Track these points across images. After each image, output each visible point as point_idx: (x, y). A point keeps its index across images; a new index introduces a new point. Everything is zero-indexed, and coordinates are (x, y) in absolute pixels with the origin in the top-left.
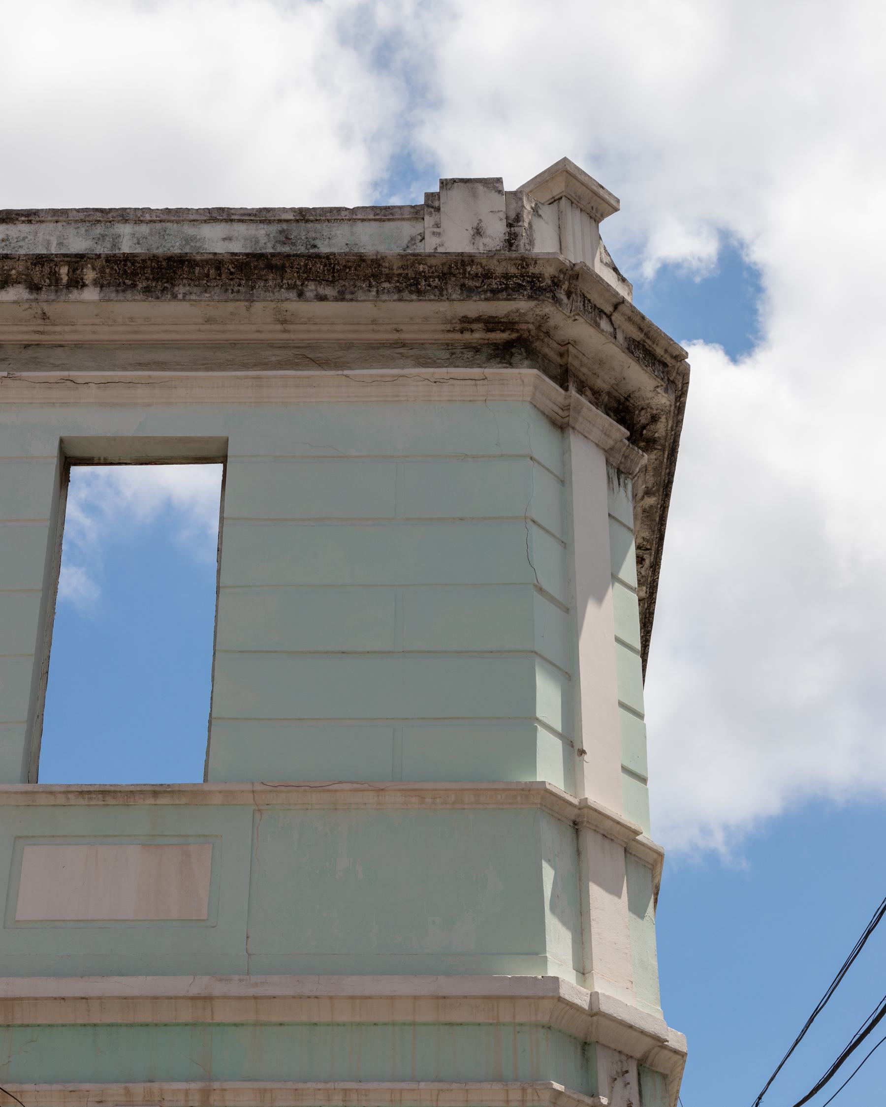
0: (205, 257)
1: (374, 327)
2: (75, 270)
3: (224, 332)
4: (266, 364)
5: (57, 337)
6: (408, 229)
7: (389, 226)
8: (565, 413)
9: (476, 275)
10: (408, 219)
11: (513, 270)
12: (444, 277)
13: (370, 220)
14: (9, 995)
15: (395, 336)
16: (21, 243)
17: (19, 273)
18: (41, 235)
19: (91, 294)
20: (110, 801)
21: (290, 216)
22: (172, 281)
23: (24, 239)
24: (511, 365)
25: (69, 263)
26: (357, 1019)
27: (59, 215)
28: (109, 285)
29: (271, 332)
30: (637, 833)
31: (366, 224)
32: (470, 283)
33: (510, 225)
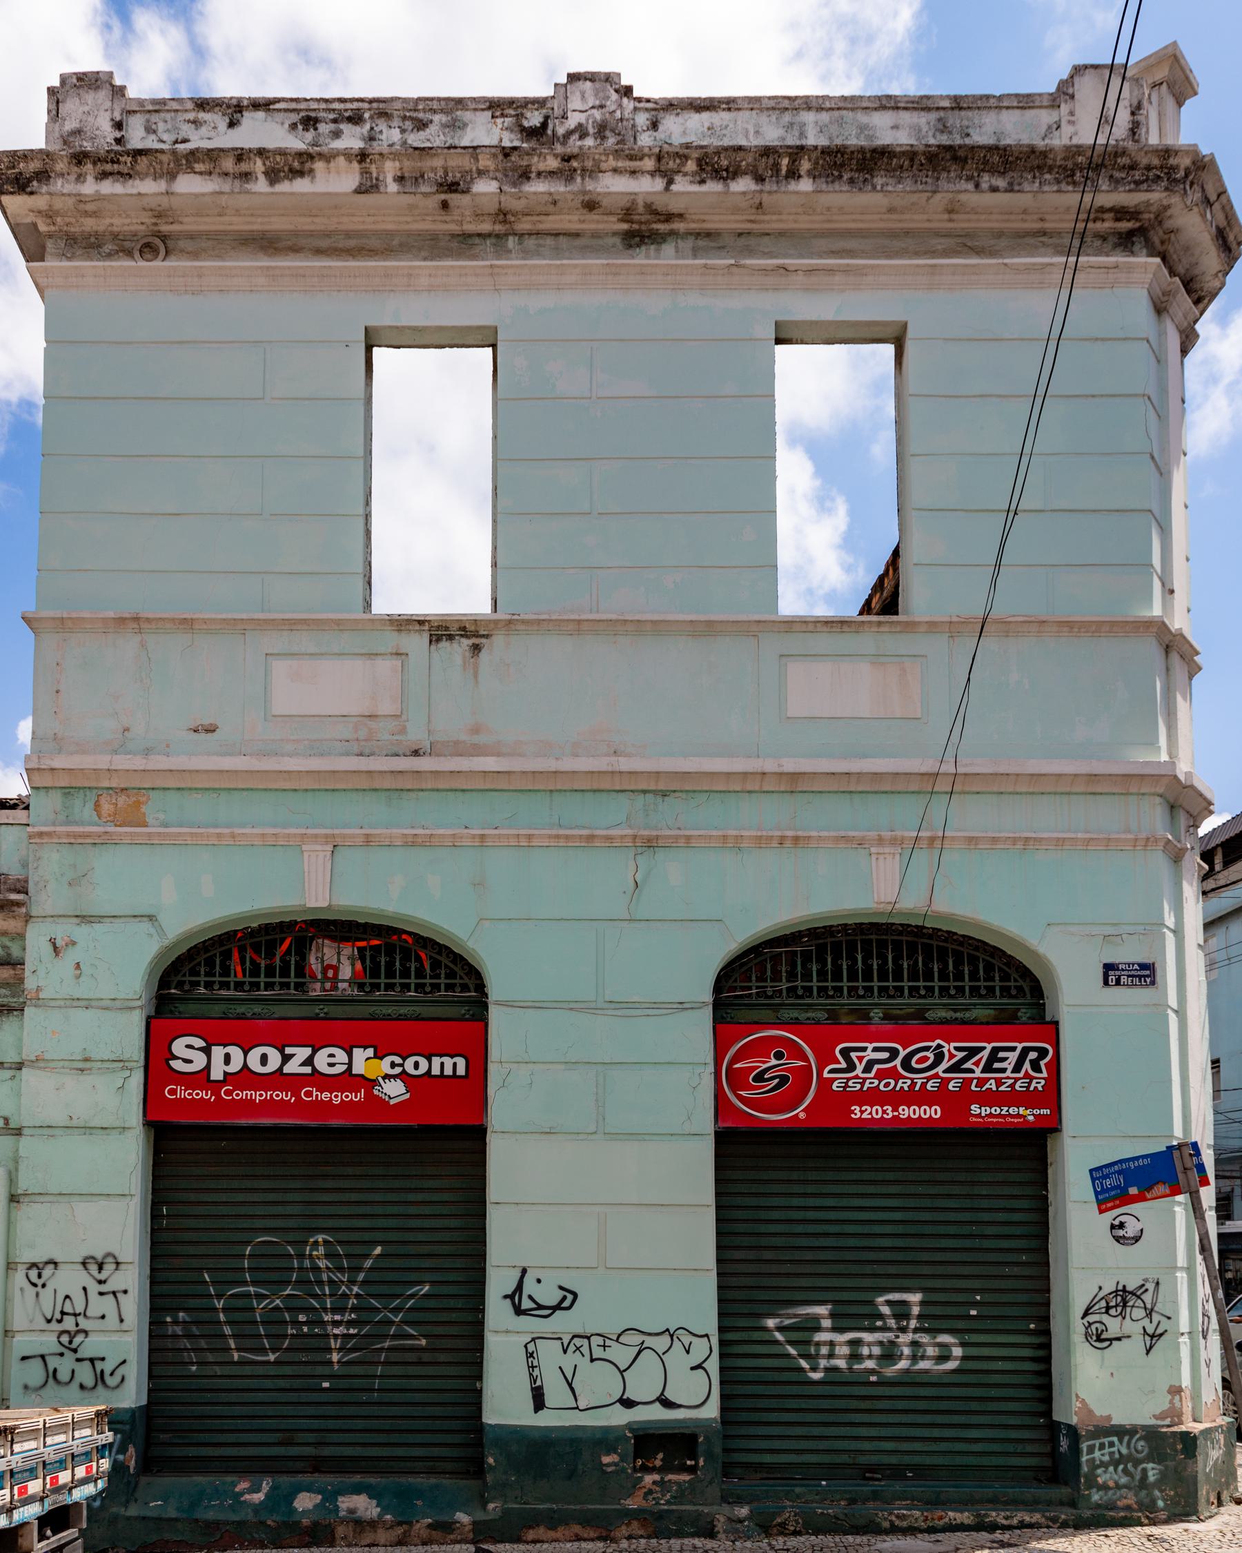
0: (904, 149)
1: (1024, 216)
2: (794, 161)
3: (900, 221)
4: (934, 252)
5: (767, 226)
6: (1046, 117)
7: (1030, 114)
8: (1166, 298)
9: (1124, 167)
10: (1046, 107)
11: (1156, 162)
12: (1098, 168)
13: (1013, 108)
14: (798, 770)
15: (1039, 225)
16: (724, 132)
17: (748, 165)
18: (739, 122)
19: (805, 185)
20: (846, 628)
21: (946, 104)
22: (871, 171)
23: (726, 127)
24: (1133, 253)
25: (790, 155)
26: (1031, 790)
27: (754, 103)
28: (820, 176)
29: (940, 221)
30: (1197, 653)
31: (1010, 111)
32: (1117, 174)
33: (1133, 114)
